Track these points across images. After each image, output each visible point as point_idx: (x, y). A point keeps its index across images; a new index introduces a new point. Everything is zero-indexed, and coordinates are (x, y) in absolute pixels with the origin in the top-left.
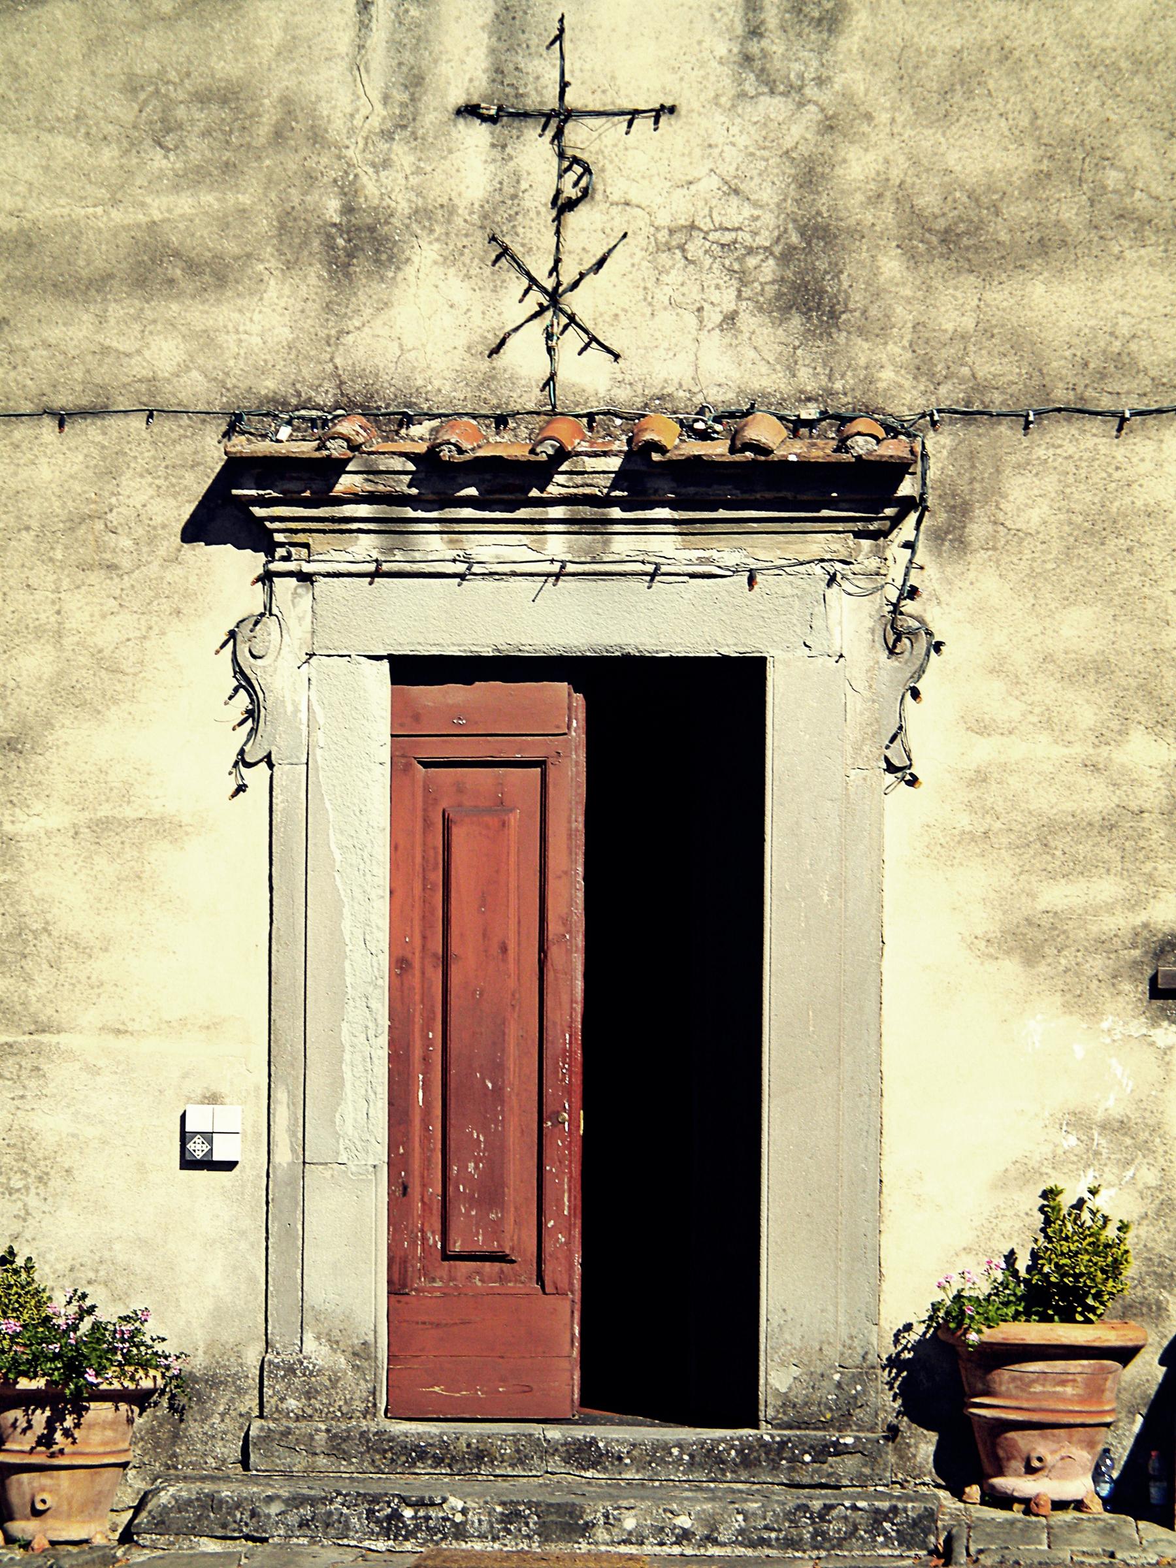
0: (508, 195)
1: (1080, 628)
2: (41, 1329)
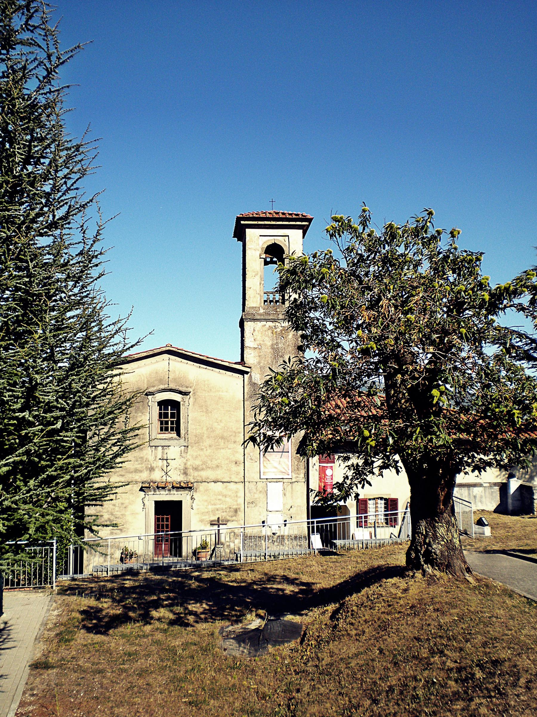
0: (163, 465)
1: (205, 498)
2: (512, 703)
